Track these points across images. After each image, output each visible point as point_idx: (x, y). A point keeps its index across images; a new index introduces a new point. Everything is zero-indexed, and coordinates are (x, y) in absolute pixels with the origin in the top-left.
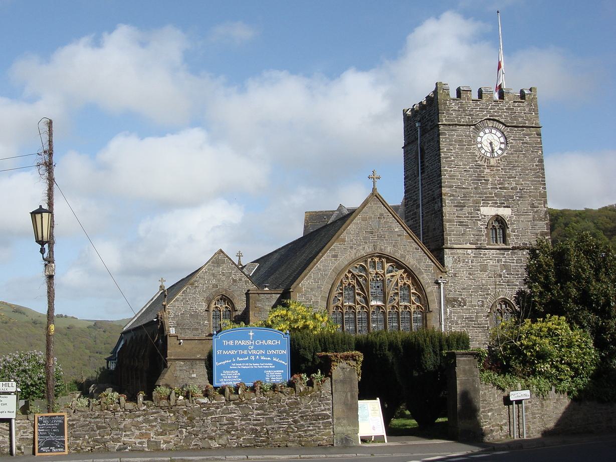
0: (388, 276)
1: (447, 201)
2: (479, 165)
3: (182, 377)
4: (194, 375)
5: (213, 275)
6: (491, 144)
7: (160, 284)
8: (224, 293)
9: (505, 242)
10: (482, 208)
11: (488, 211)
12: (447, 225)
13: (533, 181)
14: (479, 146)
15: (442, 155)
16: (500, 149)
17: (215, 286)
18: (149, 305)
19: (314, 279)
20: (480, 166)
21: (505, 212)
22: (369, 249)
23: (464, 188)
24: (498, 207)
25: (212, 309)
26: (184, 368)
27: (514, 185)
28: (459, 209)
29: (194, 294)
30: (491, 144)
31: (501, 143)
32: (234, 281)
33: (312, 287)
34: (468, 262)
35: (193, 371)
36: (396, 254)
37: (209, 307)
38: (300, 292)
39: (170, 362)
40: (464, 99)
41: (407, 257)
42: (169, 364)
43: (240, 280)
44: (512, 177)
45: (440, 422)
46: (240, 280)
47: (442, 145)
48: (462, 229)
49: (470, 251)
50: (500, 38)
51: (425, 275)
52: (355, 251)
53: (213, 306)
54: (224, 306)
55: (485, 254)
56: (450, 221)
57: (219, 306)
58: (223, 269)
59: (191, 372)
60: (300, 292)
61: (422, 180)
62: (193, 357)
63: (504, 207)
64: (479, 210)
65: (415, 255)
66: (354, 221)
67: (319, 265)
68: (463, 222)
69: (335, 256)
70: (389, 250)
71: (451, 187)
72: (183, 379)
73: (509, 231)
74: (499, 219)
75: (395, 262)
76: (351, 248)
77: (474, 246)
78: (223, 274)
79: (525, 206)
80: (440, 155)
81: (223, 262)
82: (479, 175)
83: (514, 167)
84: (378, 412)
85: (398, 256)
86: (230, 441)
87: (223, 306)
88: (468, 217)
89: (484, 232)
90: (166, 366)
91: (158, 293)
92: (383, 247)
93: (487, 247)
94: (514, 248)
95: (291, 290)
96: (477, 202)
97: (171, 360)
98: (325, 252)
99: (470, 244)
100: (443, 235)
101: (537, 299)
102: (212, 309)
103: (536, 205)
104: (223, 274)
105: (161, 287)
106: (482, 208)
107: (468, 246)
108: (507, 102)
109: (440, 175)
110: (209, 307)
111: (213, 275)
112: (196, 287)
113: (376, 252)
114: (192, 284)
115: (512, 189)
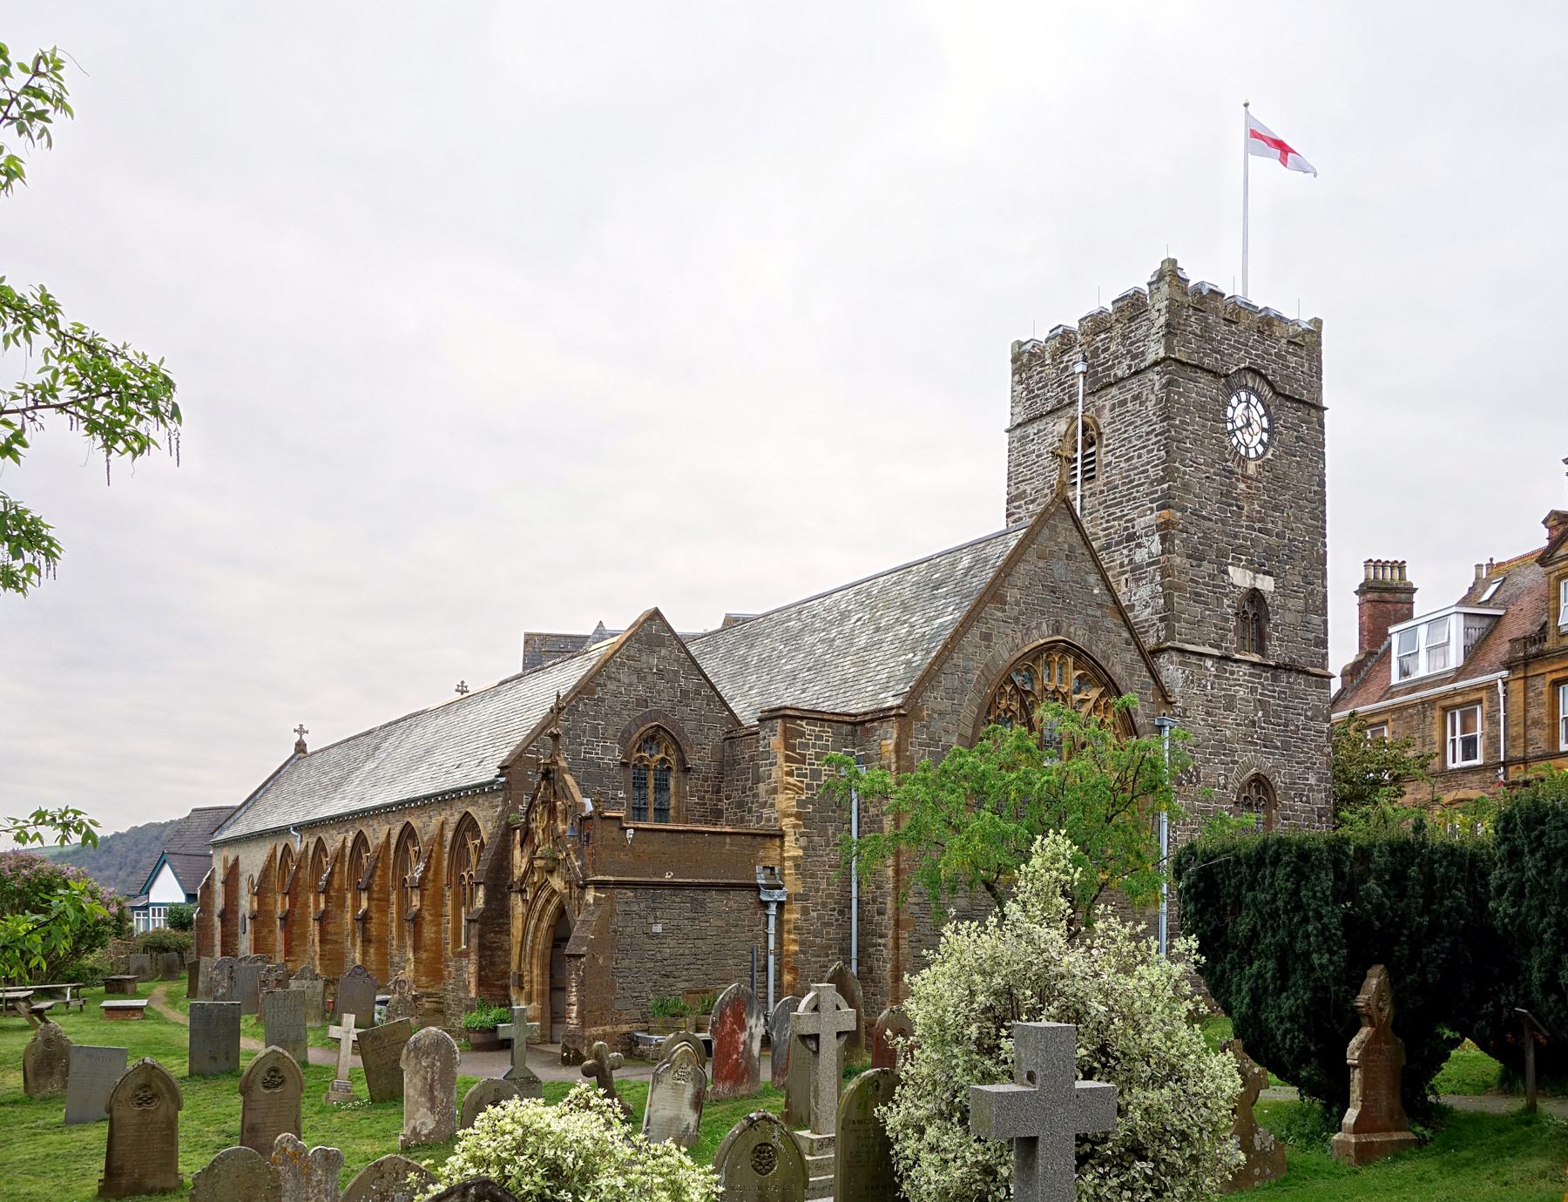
4: (658, 929)
5: (638, 672)
7: (297, 737)
9: (1261, 650)
10: (1230, 569)
11: (1240, 577)
21: (1266, 584)
23: (1204, 518)
31: (1264, 430)
32: (685, 693)
33: (942, 708)
45: (1363, 977)
46: (698, 693)
48: (1198, 608)
49: (1209, 663)
55: (1232, 673)
59: (651, 920)
61: (1082, 497)
68: (1200, 595)
69: (987, 637)
71: (1184, 510)
72: (631, 937)
74: (1255, 595)
77: (1216, 652)
81: (662, 644)
85: (1096, 652)
86: (1479, 761)
88: (1207, 585)
89: (1232, 624)
92: (1072, 630)
93: (1238, 656)
94: (1277, 667)
96: (1222, 554)
101: (516, 1171)
106: (1230, 569)
107: (1207, 650)
111: (638, 672)
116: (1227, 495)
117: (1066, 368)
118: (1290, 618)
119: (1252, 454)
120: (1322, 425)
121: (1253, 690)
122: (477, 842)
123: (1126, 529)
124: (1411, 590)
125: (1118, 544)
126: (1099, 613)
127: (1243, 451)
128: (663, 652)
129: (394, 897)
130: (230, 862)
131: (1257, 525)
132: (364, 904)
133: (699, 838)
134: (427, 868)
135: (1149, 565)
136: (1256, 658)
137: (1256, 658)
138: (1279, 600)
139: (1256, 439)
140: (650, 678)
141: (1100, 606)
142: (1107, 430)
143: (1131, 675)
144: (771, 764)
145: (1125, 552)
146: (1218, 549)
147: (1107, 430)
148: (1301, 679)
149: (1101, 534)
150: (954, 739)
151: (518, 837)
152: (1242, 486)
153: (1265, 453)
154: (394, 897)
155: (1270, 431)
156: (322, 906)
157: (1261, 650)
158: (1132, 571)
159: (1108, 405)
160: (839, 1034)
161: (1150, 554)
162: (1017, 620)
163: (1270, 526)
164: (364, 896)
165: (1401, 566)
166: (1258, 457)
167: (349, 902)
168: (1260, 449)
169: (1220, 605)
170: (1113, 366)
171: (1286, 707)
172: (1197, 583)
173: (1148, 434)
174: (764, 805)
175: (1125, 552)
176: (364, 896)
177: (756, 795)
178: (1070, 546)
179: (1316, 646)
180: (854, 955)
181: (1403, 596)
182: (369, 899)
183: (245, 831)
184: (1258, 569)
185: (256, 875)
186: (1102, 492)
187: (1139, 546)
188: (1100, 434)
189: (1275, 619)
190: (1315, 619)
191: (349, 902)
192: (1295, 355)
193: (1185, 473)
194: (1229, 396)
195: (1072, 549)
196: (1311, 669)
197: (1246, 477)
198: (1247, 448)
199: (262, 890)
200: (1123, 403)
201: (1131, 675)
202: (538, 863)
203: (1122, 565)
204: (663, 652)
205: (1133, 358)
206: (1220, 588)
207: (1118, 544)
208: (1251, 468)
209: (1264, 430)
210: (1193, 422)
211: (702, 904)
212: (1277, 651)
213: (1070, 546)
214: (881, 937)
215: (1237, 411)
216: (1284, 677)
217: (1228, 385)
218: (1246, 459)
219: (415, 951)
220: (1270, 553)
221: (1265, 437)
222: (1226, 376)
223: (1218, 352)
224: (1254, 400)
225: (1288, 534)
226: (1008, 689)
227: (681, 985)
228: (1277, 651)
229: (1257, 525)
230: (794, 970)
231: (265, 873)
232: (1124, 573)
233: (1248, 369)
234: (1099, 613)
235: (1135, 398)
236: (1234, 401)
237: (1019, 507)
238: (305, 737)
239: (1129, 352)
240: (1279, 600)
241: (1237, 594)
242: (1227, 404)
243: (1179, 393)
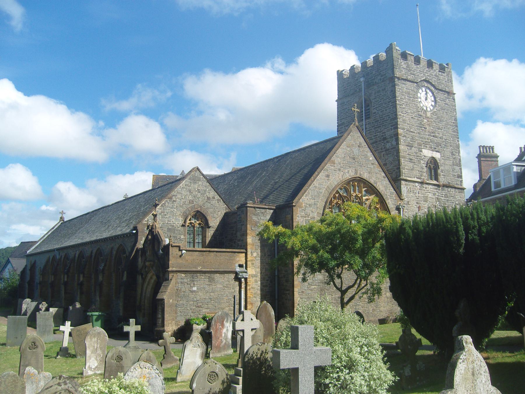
0: (364, 198)
1: (402, 139)
2: (421, 113)
3: (183, 289)
4: (195, 289)
6: (426, 99)
8: (199, 209)
9: (436, 179)
10: (423, 150)
11: (427, 153)
12: (402, 160)
13: (452, 134)
14: (419, 100)
15: (398, 102)
16: (432, 105)
17: (191, 202)
18: (50, 232)
19: (312, 196)
20: (421, 116)
21: (437, 156)
22: (350, 174)
23: (412, 132)
24: (433, 151)
25: (187, 224)
26: (185, 281)
27: (441, 135)
28: (409, 148)
29: (172, 208)
30: (426, 99)
32: (208, 198)
33: (310, 203)
34: (416, 193)
35: (194, 284)
36: (371, 180)
37: (185, 222)
38: (301, 207)
39: (172, 274)
40: (409, 61)
41: (378, 183)
42: (170, 276)
43: (214, 198)
44: (440, 129)
46: (214, 198)
47: (398, 94)
48: (411, 165)
49: (417, 184)
50: (418, 26)
51: (389, 201)
52: (342, 173)
53: (188, 222)
54: (198, 222)
55: (426, 188)
56: (404, 157)
57: (193, 222)
58: (199, 186)
59: (192, 285)
60: (301, 207)
61: (366, 125)
62: (194, 269)
63: (436, 151)
64: (421, 151)
65: (383, 185)
66: (341, 147)
67: (316, 183)
69: (328, 176)
70: (365, 176)
71: (403, 129)
72: (184, 292)
73: (439, 171)
74: (433, 158)
75: (370, 187)
76: (339, 170)
77: (419, 180)
78: (199, 191)
79: (448, 153)
80: (396, 101)
82: (421, 123)
83: (440, 121)
84: (178, 325)
85: (372, 181)
87: (197, 223)
89: (425, 170)
90: (167, 279)
91: (59, 223)
92: (362, 173)
94: (445, 186)
95: (294, 204)
97: (173, 272)
98: (321, 171)
99: (417, 178)
100: (399, 168)
102: (187, 224)
103: (454, 153)
104: (199, 191)
105: (61, 218)
106: (423, 150)
107: (415, 179)
108: (435, 71)
109: (396, 118)
110: (185, 222)
112: (174, 201)
113: (357, 176)
114: (171, 198)
115: (440, 138)
116: (421, 126)
117: (357, 80)
118: (447, 168)
119: (429, 109)
120: (454, 99)
121: (434, 194)
122: (125, 255)
123: (382, 136)
124: (497, 157)
125: (380, 141)
126: (372, 167)
127: (425, 108)
128: (200, 183)
129: (93, 276)
130: (33, 262)
131: (432, 134)
132: (81, 279)
133: (212, 254)
134: (105, 265)
135: (392, 149)
136: (435, 182)
137: (435, 182)
138: (442, 161)
139: (430, 104)
140: (194, 193)
141: (373, 164)
142: (373, 101)
143: (386, 190)
144: (242, 225)
145: (383, 144)
146: (418, 143)
147: (373, 101)
148: (453, 190)
149: (373, 137)
150: (316, 214)
151: (140, 253)
152: (425, 121)
153: (433, 109)
154: (93, 276)
155: (435, 101)
156: (66, 280)
157: (436, 179)
158: (386, 151)
159: (373, 92)
160: (252, 330)
161: (392, 145)
162: (339, 170)
163: (437, 135)
164: (81, 276)
165: (492, 148)
166: (431, 110)
167: (76, 278)
168: (432, 108)
169: (420, 163)
170: (374, 79)
171: (448, 200)
172: (410, 155)
173: (389, 102)
174: (239, 240)
175: (383, 144)
176: (81, 276)
177: (237, 237)
178: (360, 143)
179: (458, 177)
180: (276, 297)
181: (494, 159)
182: (84, 277)
183: (80, 241)
184: (434, 150)
185: (42, 268)
186: (373, 123)
187: (388, 142)
188: (371, 102)
189: (441, 168)
190: (457, 168)
191: (76, 278)
192: (442, 75)
193: (403, 116)
194: (418, 90)
195: (360, 144)
196: (456, 186)
197: (427, 118)
198: (426, 107)
199: (44, 272)
200: (379, 92)
201: (386, 190)
202: (147, 264)
203: (382, 149)
204: (200, 183)
205: (381, 76)
206: (420, 158)
207: (380, 141)
208: (429, 114)
209: (432, 101)
210: (405, 98)
211: (213, 279)
212: (442, 180)
213: (360, 143)
214: (287, 290)
215: (422, 94)
216: (446, 189)
217: (418, 86)
218: (426, 111)
219: (100, 297)
220: (438, 144)
221: (433, 104)
222: (417, 83)
223: (413, 74)
224: (428, 91)
225: (444, 137)
226: (337, 195)
227: (204, 311)
228: (442, 180)
229: (432, 134)
230: (252, 304)
231: (45, 266)
232: (383, 151)
233: (423, 80)
234: (372, 167)
235: (383, 90)
236: (420, 91)
237: (342, 128)
238: (64, 216)
239: (380, 74)
240: (442, 161)
241: (426, 160)
242: (418, 92)
243: (399, 88)
